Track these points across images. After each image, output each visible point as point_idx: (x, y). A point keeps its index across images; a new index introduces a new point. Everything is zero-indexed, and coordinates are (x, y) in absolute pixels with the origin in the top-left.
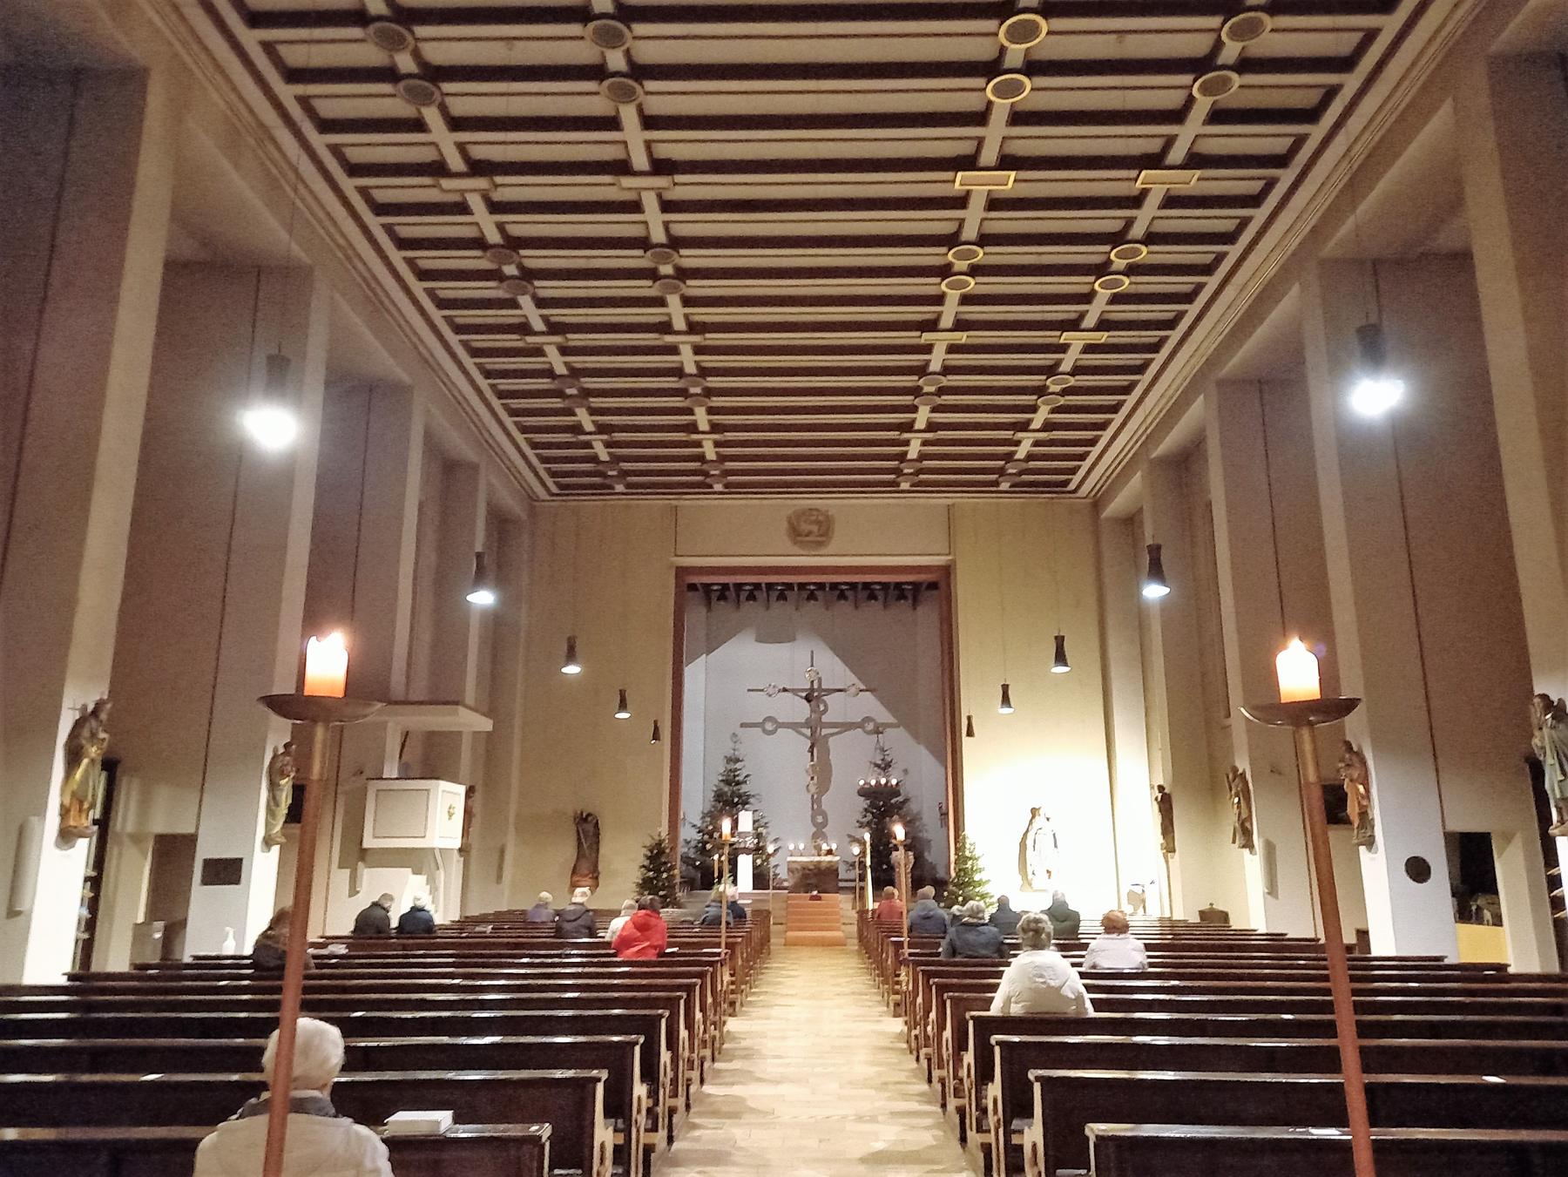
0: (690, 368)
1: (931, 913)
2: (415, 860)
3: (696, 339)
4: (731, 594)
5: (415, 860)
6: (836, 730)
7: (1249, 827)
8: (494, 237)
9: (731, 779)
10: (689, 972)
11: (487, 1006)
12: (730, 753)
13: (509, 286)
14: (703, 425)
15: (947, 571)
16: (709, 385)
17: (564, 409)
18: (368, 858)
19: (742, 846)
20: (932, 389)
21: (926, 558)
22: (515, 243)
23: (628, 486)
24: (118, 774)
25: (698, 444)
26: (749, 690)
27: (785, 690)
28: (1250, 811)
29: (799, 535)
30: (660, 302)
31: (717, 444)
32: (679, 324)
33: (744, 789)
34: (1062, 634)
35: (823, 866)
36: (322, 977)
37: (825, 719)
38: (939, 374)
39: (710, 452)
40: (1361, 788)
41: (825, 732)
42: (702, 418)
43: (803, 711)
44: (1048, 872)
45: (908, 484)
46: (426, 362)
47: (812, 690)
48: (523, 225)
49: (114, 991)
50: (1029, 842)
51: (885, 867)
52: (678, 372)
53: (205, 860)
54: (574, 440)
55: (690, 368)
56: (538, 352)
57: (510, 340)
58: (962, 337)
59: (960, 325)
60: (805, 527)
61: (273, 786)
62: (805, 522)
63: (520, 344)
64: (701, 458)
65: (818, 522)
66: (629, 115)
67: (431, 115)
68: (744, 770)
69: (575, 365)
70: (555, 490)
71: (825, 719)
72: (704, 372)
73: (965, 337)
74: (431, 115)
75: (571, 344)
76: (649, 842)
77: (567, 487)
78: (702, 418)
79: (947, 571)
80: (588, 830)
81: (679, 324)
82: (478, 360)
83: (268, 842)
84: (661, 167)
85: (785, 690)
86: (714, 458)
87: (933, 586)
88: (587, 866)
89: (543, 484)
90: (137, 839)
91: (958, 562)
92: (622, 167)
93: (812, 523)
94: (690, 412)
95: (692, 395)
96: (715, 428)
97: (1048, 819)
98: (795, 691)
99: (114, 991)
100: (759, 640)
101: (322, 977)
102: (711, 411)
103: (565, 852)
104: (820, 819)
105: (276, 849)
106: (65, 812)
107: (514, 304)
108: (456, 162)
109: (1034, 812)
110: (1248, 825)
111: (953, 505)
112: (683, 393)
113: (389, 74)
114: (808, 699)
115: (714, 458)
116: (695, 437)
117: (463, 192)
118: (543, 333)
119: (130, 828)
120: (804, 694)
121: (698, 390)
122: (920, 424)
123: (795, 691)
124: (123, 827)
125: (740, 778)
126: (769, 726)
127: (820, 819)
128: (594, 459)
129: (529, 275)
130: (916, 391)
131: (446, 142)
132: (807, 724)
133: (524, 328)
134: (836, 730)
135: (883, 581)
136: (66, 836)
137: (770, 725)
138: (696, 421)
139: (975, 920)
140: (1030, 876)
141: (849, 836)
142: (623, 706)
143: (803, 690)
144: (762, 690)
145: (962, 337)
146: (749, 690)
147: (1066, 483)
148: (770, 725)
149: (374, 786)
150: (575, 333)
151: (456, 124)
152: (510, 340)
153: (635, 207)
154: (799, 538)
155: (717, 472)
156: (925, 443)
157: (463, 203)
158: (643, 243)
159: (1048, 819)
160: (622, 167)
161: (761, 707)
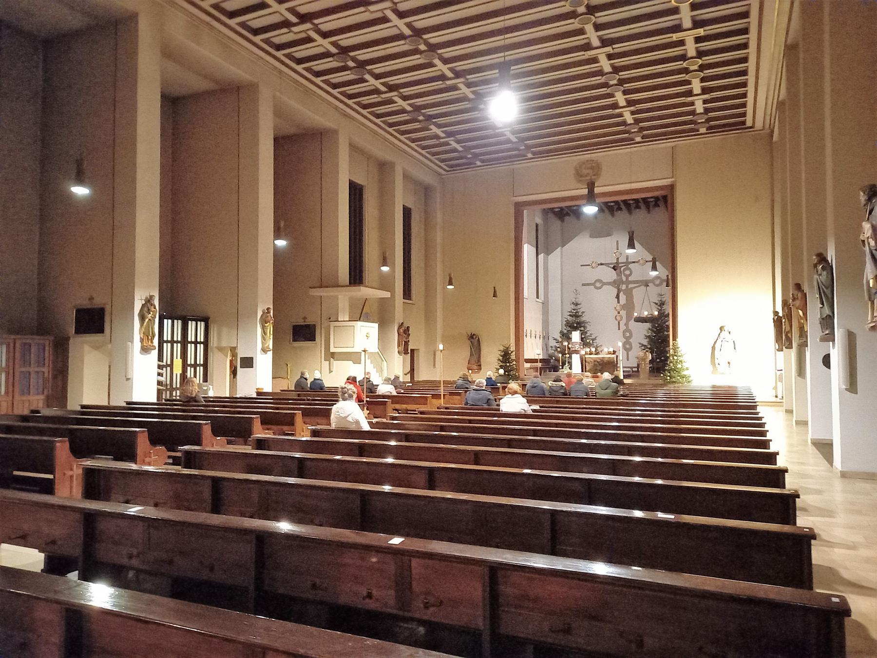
0: (607, 68)
1: (536, 385)
2: (354, 357)
3: (608, 49)
4: (642, 205)
5: (354, 357)
6: (637, 285)
7: (790, 336)
8: (407, 32)
9: (576, 315)
10: (241, 406)
11: (683, 431)
12: (574, 300)
13: (426, 56)
14: (697, 89)
15: (672, 188)
16: (621, 77)
17: (421, 128)
18: (336, 356)
19: (574, 349)
20: (696, 67)
21: (651, 182)
22: (417, 109)
23: (534, 153)
24: (209, 322)
25: (621, 115)
26: (582, 266)
27: (602, 264)
28: (791, 327)
29: (581, 176)
30: (581, 32)
31: (633, 113)
32: (596, 42)
33: (583, 319)
34: (632, 230)
35: (605, 360)
36: (166, 405)
37: (630, 279)
38: (695, 58)
39: (629, 118)
40: (801, 313)
41: (630, 286)
42: (621, 99)
43: (611, 275)
44: (729, 363)
45: (705, 129)
46: (345, 115)
47: (617, 263)
48: (419, 101)
49: (147, 409)
50: (717, 346)
51: (663, 358)
52: (600, 73)
53: (241, 358)
54: (438, 142)
55: (607, 68)
56: (454, 88)
57: (610, 112)
58: (701, 32)
59: (700, 54)
60: (585, 172)
61: (264, 328)
62: (585, 169)
63: (379, 99)
64: (624, 123)
65: (592, 168)
66: (589, 28)
67: (437, 61)
68: (582, 309)
69: (416, 104)
70: (448, 169)
71: (630, 279)
72: (616, 70)
73: (702, 31)
74: (437, 61)
75: (616, 51)
76: (502, 348)
77: (451, 166)
78: (621, 99)
79: (672, 188)
80: (475, 342)
81: (596, 42)
82: (472, 89)
83: (264, 350)
84: (605, 43)
85: (602, 264)
86: (632, 122)
87: (665, 198)
88: (476, 363)
89: (440, 167)
90: (220, 349)
91: (678, 184)
92: (587, 47)
93: (588, 168)
94: (611, 96)
95: (612, 86)
96: (630, 103)
97: (730, 333)
98: (607, 265)
99: (147, 409)
100: (591, 237)
101: (166, 405)
102: (625, 93)
103: (464, 353)
104: (628, 334)
105: (270, 354)
106: (142, 340)
107: (431, 65)
108: (449, 74)
109: (721, 329)
110: (789, 335)
111: (675, 146)
112: (606, 85)
113: (416, 52)
114: (614, 268)
115: (632, 122)
116: (617, 111)
117: (382, 10)
118: (386, 92)
119: (215, 345)
120: (612, 266)
121: (615, 82)
122: (697, 89)
123: (607, 265)
124: (213, 344)
125: (580, 314)
126: (598, 285)
127: (628, 334)
128: (455, 150)
129: (429, 118)
130: (686, 71)
131: (445, 69)
132: (615, 282)
133: (443, 77)
134: (637, 285)
135: (560, 206)
136: (145, 350)
137: (598, 284)
138: (617, 100)
139: (478, 388)
140: (717, 365)
141: (640, 344)
142: (450, 283)
143: (611, 264)
144: (589, 265)
145: (701, 32)
146: (582, 266)
147: (744, 123)
148: (598, 284)
149: (333, 324)
150: (403, 88)
151: (446, 61)
152: (610, 112)
153: (595, 60)
154: (581, 179)
155: (636, 130)
156: (705, 102)
157: (384, 17)
158: (600, 73)
159: (730, 333)
160: (587, 47)
161: (592, 275)
